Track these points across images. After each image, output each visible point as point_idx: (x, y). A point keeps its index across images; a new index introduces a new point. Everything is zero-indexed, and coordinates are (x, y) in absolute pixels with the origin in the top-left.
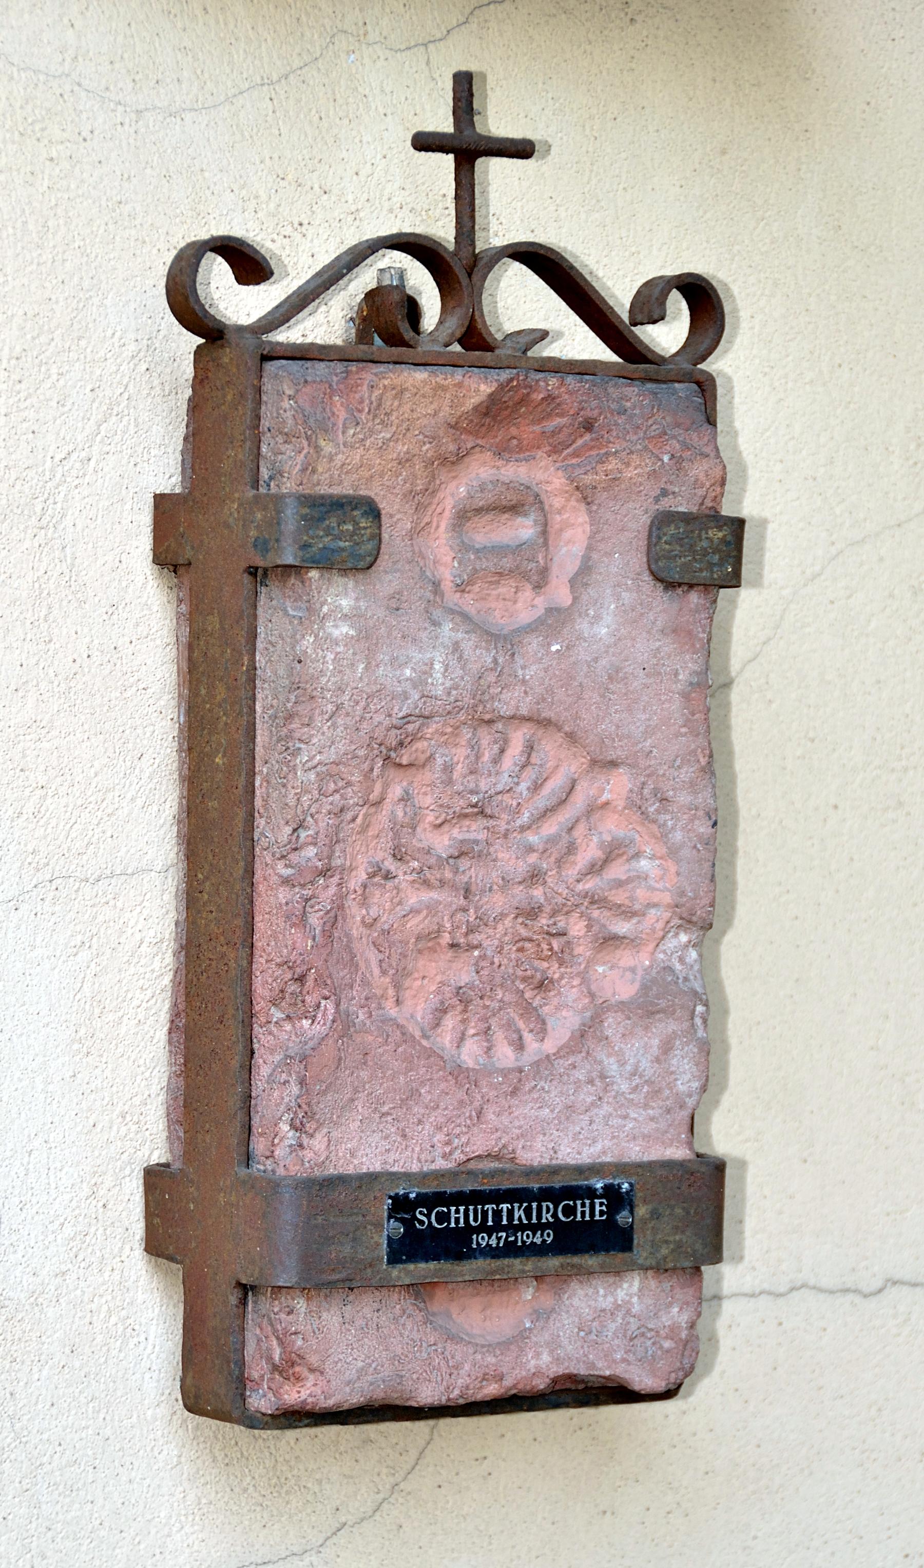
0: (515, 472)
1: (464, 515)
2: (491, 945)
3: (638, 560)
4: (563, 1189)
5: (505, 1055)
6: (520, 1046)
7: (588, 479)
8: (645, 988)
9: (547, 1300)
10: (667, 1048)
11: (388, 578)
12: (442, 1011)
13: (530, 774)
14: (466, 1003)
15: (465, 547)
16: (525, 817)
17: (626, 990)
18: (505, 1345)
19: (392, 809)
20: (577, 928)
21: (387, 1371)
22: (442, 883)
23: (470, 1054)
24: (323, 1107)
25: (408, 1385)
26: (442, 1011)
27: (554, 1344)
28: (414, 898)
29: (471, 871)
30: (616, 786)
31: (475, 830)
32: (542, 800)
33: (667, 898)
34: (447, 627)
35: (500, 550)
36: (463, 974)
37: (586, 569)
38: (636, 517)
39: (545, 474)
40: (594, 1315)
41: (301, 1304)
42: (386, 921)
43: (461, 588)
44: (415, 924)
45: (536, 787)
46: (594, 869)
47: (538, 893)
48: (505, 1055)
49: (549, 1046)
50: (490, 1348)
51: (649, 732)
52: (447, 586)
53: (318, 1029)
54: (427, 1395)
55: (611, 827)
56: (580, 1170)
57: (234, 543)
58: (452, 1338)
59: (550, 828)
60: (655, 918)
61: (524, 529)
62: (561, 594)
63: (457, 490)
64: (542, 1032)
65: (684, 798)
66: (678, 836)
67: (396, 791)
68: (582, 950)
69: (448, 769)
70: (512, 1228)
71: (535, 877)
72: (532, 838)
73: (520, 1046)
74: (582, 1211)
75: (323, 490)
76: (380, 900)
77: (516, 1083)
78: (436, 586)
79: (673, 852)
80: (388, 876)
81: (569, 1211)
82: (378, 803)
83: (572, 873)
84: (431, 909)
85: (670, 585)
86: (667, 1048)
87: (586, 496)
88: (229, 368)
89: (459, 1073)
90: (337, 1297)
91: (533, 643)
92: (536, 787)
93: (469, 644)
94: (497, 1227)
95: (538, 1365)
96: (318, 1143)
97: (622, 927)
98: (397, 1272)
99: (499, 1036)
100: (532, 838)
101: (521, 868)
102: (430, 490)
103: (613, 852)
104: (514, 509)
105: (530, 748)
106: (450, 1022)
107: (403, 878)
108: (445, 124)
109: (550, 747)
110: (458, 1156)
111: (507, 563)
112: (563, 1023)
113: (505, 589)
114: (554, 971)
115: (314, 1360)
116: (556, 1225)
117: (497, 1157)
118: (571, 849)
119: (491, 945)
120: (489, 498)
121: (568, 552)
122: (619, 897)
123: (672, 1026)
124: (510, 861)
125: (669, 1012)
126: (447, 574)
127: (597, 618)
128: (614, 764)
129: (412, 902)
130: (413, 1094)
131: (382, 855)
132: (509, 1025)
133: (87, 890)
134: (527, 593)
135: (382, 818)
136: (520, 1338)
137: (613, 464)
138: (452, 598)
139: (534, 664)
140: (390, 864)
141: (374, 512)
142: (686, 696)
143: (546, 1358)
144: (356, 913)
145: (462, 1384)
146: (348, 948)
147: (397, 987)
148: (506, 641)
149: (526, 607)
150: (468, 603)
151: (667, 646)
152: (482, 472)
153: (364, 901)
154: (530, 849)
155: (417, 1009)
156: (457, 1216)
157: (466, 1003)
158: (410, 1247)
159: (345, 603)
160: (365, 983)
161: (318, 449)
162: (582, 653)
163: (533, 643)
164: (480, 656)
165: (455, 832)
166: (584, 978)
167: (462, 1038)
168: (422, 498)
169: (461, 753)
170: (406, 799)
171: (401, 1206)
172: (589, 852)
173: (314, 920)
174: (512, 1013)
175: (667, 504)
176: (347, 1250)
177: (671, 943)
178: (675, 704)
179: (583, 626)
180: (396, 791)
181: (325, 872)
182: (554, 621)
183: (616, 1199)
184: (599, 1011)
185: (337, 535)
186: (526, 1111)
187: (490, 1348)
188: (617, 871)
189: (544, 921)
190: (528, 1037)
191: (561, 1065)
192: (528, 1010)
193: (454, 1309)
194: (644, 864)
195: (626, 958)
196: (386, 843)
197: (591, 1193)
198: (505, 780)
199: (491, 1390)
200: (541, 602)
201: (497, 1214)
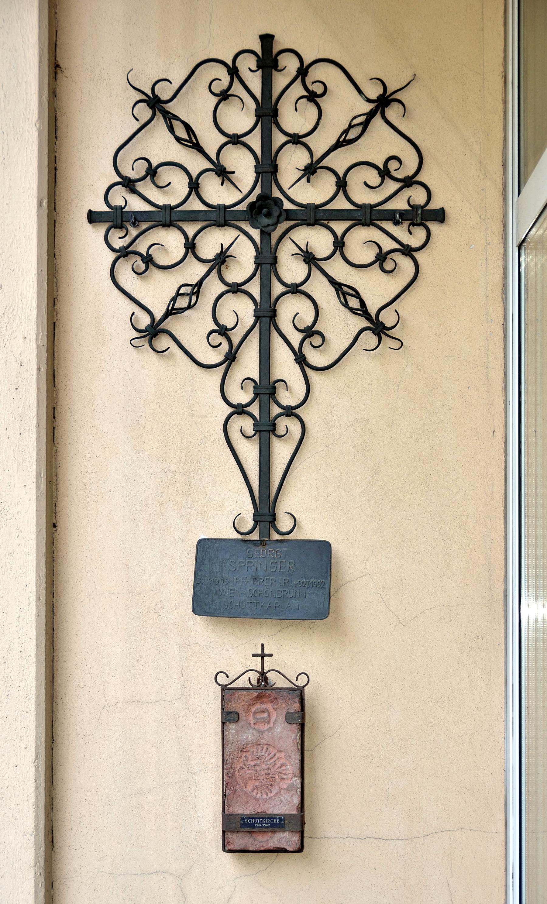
0: (264, 706)
1: (255, 713)
2: (261, 779)
3: (284, 719)
4: (272, 817)
5: (265, 796)
6: (267, 795)
7: (275, 707)
8: (288, 786)
9: (273, 835)
10: (292, 796)
11: (241, 723)
12: (253, 789)
13: (267, 753)
14: (257, 788)
15: (255, 718)
16: (267, 759)
17: (285, 787)
18: (265, 842)
19: (243, 758)
20: (277, 777)
21: (244, 844)
22: (252, 770)
23: (259, 796)
24: (231, 803)
25: (248, 847)
26: (253, 789)
27: (273, 842)
28: (248, 772)
29: (257, 768)
30: (282, 755)
31: (258, 762)
32: (269, 757)
33: (291, 772)
34: (251, 730)
35: (261, 718)
36: (257, 784)
37: (275, 721)
38: (284, 713)
39: (269, 706)
40: (286, 838)
41: (229, 834)
42: (242, 775)
43: (254, 724)
44: (248, 776)
45: (268, 755)
46: (279, 768)
47: (269, 771)
48: (265, 796)
49: (272, 795)
50: (262, 842)
51: (287, 746)
52: (252, 724)
53: (231, 791)
54: (251, 849)
55: (282, 761)
56: (275, 815)
57: (229, 717)
58: (255, 840)
59: (272, 761)
60: (290, 775)
61: (266, 715)
62: (271, 725)
63: (253, 709)
64: (271, 792)
65: (293, 757)
66: (293, 762)
67: (244, 755)
68: (278, 780)
69: (253, 752)
70: (262, 823)
71: (268, 769)
72: (268, 763)
73: (267, 795)
74: (275, 821)
75: (229, 710)
76: (242, 772)
77: (266, 801)
78: (250, 724)
79: (292, 765)
80: (243, 768)
81: (272, 821)
82: (241, 757)
83: (275, 768)
84: (251, 773)
85: (289, 723)
86: (292, 796)
87: (275, 709)
88: (227, 691)
89: (256, 799)
90: (235, 833)
91: (266, 733)
92: (268, 755)
93: (255, 733)
94: (260, 823)
95: (271, 845)
96: (231, 809)
97: (285, 777)
98: (242, 829)
99: (264, 793)
100: (268, 763)
101: (266, 767)
102: (249, 710)
103: (282, 766)
104: (264, 712)
105: (267, 749)
106: (255, 791)
107: (246, 769)
108: (260, 652)
109: (271, 749)
110: (256, 812)
111: (262, 720)
112: (275, 790)
113: (263, 724)
114: (273, 783)
115: (232, 842)
116: (270, 823)
117: (263, 812)
118: (275, 764)
119: (261, 779)
120: (259, 710)
121: (273, 719)
122: (284, 772)
123: (293, 792)
124: (264, 766)
125: (292, 790)
126: (252, 722)
127: (278, 729)
128: (281, 751)
129: (248, 773)
130: (248, 802)
131: (242, 765)
132: (265, 792)
133: (213, 769)
134: (266, 725)
135: (241, 760)
136: (268, 840)
137: (279, 705)
138: (253, 726)
139: (267, 736)
140: (244, 767)
141: (238, 714)
142: (293, 741)
143: (272, 844)
144: (237, 774)
145: (257, 848)
146: (236, 779)
147: (245, 786)
148: (262, 733)
149: (266, 727)
150: (256, 727)
151: (290, 733)
152: (258, 706)
153: (239, 772)
154: (268, 764)
155: (249, 788)
156: (253, 821)
157: (257, 788)
158: (244, 825)
159: (234, 727)
160: (239, 785)
161: (228, 704)
162: (275, 734)
163: (266, 733)
164: (257, 735)
165: (255, 762)
166: (278, 784)
167: (257, 794)
168: (247, 711)
169: (255, 749)
170: (246, 756)
171: (243, 819)
172: (278, 765)
173: (230, 775)
174: (266, 790)
175: (289, 711)
176: (234, 825)
177: (293, 779)
178: (292, 742)
179: (275, 730)
180: (244, 755)
181: (231, 768)
182: (270, 729)
183: (281, 820)
184: (280, 790)
185: (232, 717)
186: (267, 805)
187: (262, 842)
188: (283, 768)
189: (271, 776)
190: (269, 794)
191: (274, 798)
192: (268, 789)
193: (257, 836)
194: (288, 767)
195: (286, 782)
196: (242, 763)
197: (276, 818)
198: (263, 754)
199: (263, 849)
200: (269, 726)
201: (260, 821)
